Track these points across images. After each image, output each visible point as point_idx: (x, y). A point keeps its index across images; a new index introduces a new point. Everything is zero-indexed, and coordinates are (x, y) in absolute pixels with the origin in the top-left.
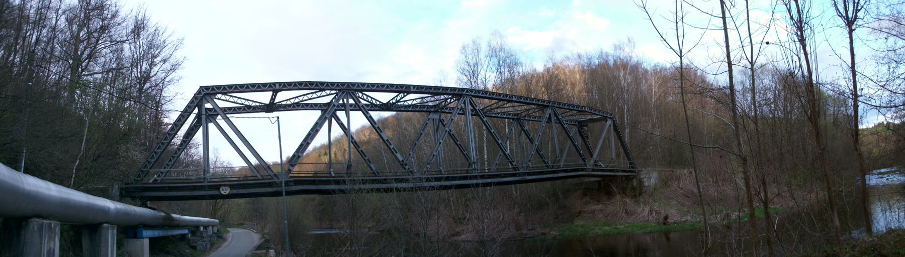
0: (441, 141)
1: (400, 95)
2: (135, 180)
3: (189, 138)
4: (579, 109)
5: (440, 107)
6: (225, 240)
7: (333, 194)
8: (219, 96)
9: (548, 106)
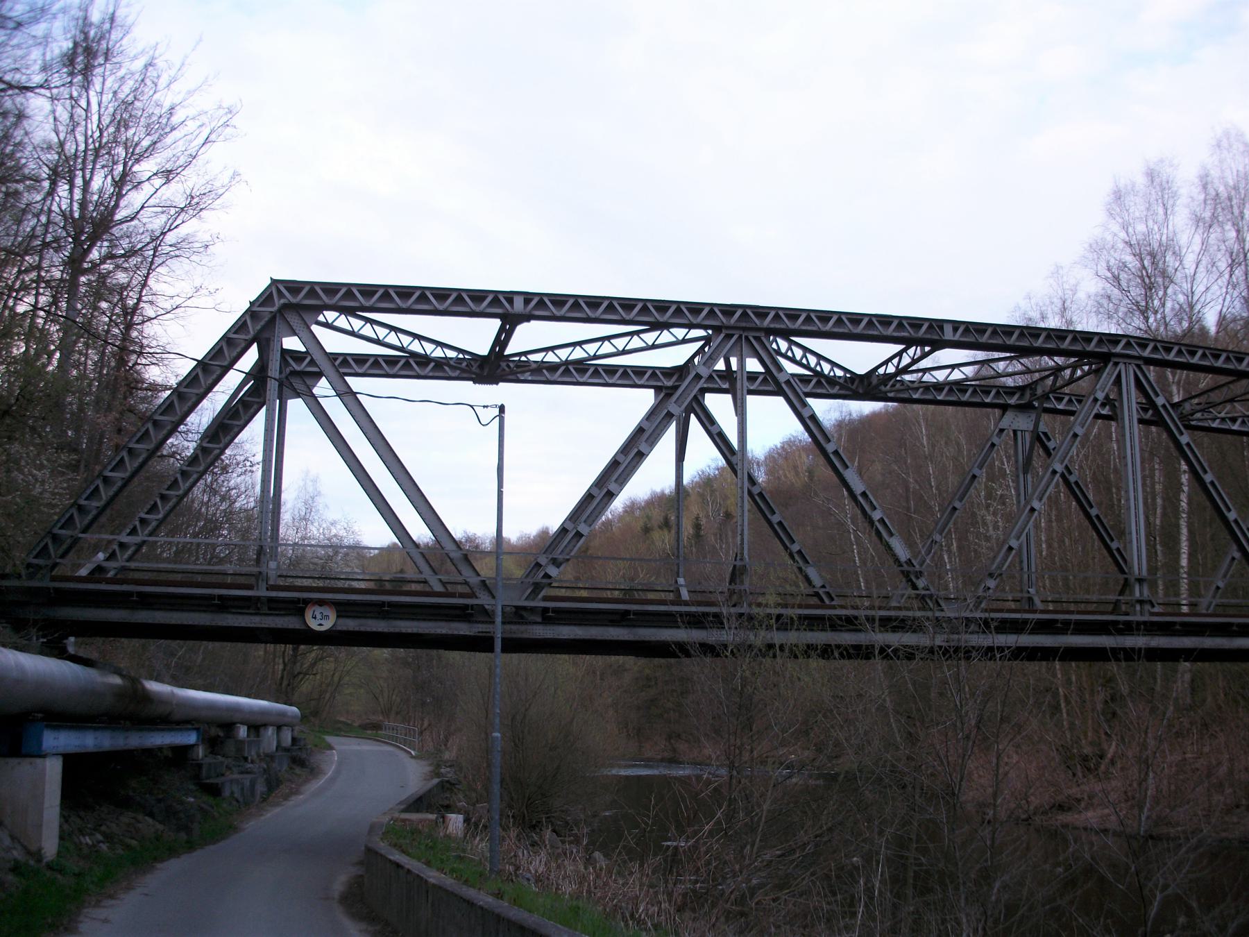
0: (1036, 504)
1: (911, 351)
2: (29, 566)
3: (219, 442)
5: (1039, 391)
6: (314, 772)
7: (679, 657)
8: (330, 316)
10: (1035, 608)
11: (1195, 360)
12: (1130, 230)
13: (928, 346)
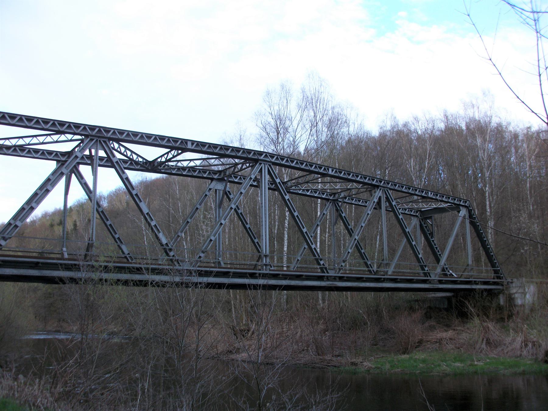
0: (223, 222)
1: (173, 152)
4: (423, 194)
5: (227, 173)
7: (60, 284)
9: (378, 187)
10: (221, 266)
11: (293, 164)
12: (272, 108)
13: (180, 150)
